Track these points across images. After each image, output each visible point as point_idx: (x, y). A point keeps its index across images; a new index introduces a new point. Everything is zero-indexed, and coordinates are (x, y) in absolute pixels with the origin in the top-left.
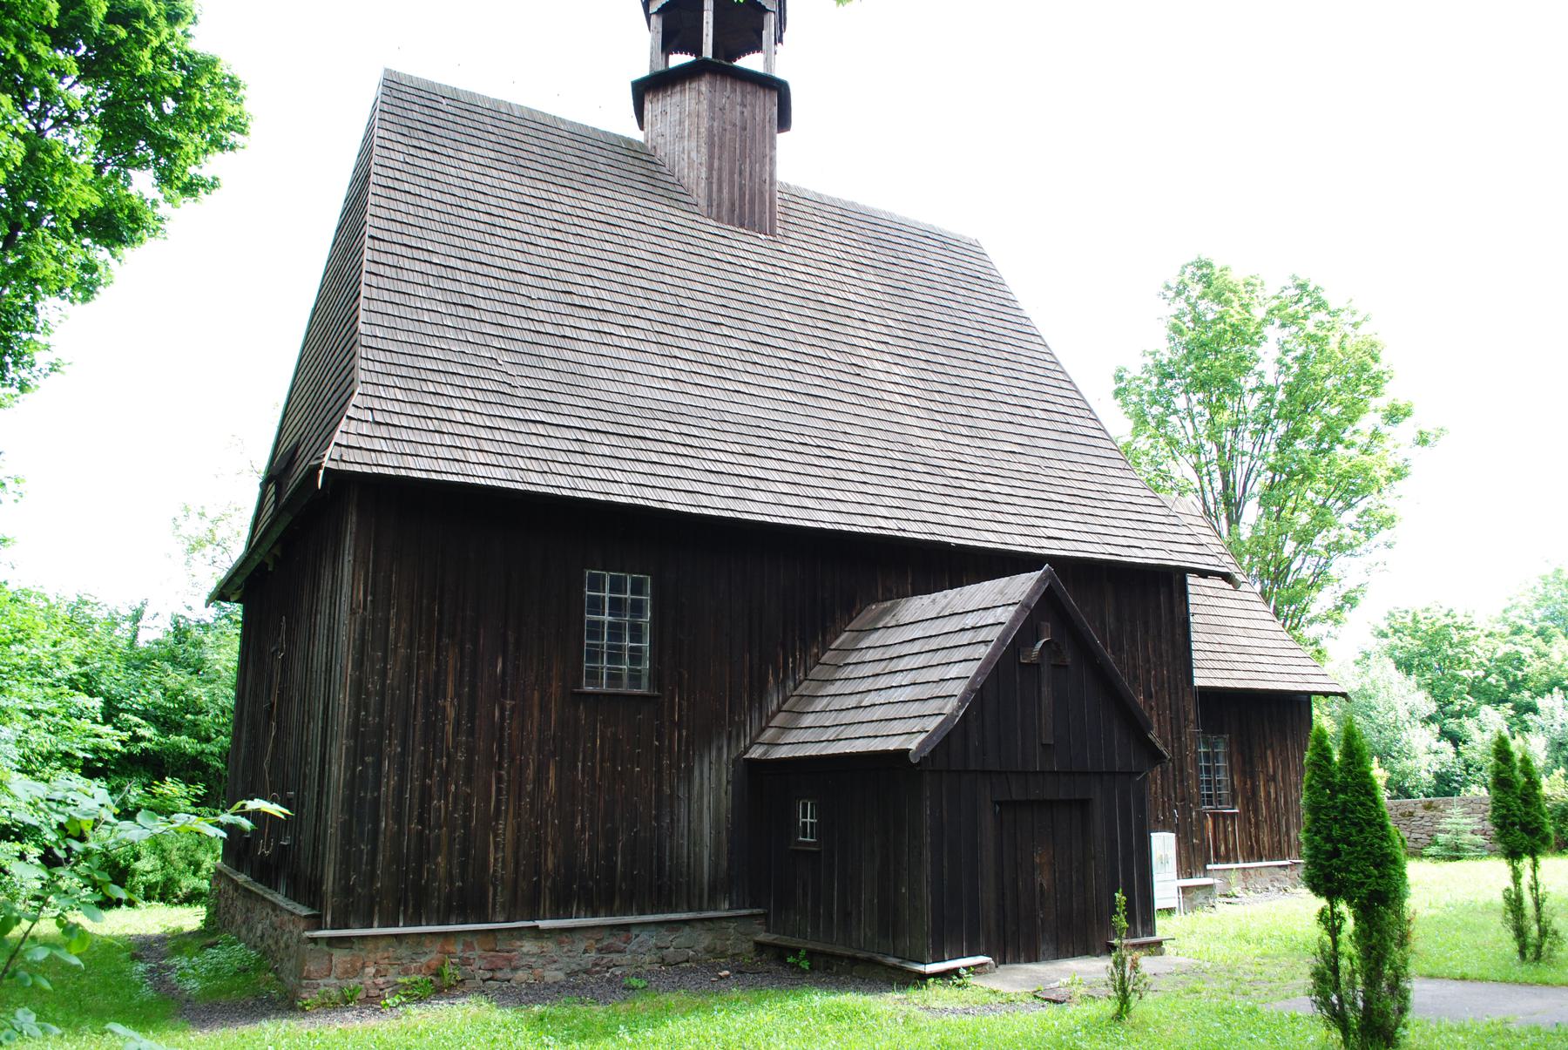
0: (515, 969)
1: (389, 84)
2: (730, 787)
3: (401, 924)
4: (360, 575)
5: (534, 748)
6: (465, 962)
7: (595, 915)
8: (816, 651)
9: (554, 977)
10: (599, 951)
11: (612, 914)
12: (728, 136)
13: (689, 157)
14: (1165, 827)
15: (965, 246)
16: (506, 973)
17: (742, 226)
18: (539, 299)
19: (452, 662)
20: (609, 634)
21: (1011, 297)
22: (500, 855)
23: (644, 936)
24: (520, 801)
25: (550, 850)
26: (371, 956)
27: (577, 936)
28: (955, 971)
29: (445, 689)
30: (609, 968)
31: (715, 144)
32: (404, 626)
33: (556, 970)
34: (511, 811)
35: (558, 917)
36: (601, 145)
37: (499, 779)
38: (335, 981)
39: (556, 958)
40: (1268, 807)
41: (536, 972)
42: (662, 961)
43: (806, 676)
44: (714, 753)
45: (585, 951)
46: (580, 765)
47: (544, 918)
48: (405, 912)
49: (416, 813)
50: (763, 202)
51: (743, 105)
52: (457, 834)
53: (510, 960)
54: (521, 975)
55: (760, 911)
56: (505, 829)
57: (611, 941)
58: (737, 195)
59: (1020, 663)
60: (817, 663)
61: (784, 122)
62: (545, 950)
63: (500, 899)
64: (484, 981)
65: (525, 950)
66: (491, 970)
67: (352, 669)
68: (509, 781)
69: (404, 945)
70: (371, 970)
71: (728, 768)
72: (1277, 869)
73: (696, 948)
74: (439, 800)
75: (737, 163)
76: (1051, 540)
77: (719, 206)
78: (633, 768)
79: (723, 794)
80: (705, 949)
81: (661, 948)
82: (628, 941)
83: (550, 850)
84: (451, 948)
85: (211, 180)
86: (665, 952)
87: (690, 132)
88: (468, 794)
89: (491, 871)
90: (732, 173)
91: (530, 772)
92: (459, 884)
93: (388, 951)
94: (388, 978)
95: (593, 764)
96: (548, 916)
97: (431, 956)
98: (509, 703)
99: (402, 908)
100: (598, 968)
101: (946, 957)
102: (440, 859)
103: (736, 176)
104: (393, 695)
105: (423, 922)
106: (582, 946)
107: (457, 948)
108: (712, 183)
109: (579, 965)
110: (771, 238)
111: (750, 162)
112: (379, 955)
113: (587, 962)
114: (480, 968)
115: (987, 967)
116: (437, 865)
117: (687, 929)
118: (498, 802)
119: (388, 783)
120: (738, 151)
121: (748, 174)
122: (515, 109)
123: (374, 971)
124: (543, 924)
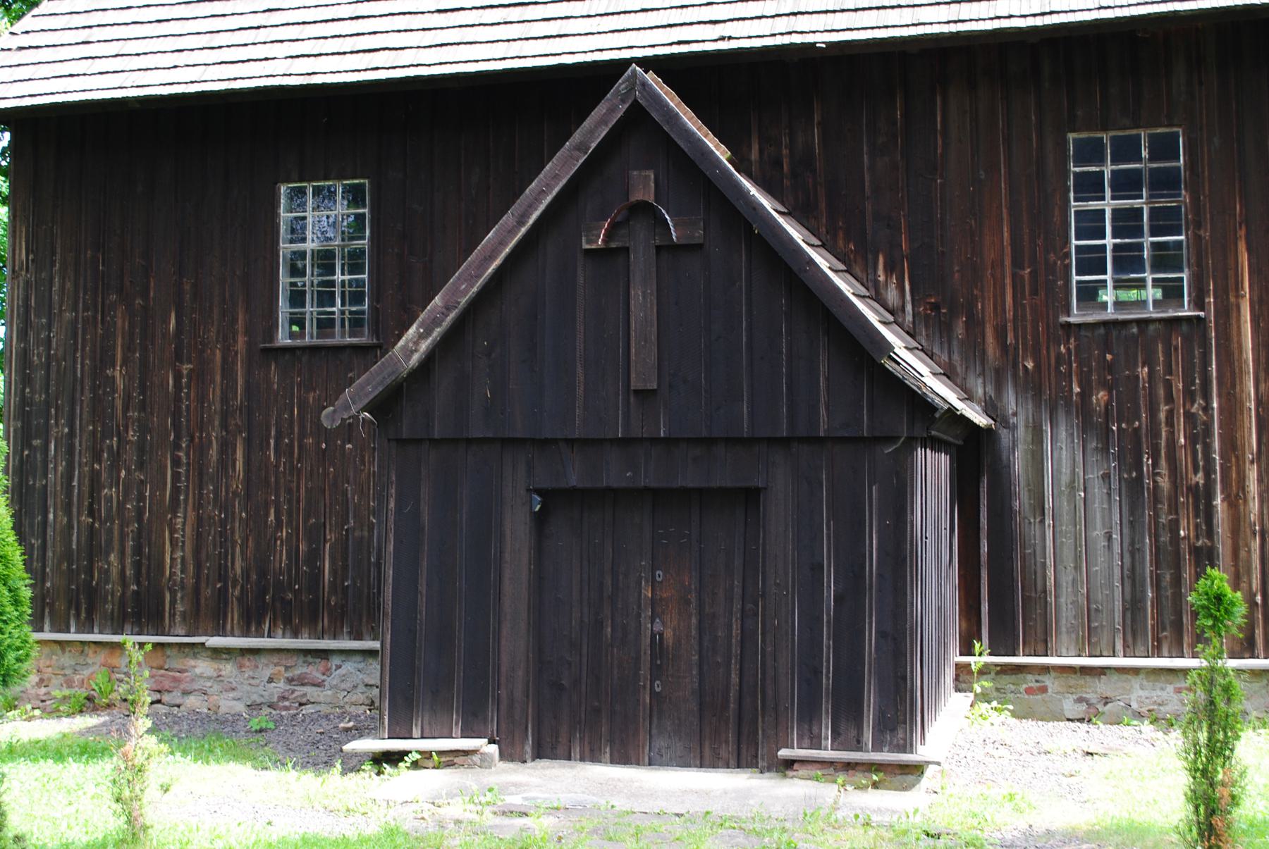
0: (186, 693)
3: (73, 629)
4: (21, 232)
5: (217, 423)
7: (296, 634)
10: (290, 681)
19: (121, 322)
22: (179, 554)
23: (349, 666)
24: (201, 488)
25: (238, 550)
27: (263, 660)
29: (114, 355)
32: (68, 285)
33: (234, 699)
34: (191, 501)
35: (246, 633)
37: (176, 462)
39: (234, 684)
45: (271, 680)
46: (272, 442)
48: (78, 615)
49: (86, 503)
52: (130, 529)
54: (192, 701)
56: (184, 524)
57: (305, 670)
62: (223, 673)
63: (180, 607)
65: (198, 671)
66: (159, 691)
68: (188, 464)
69: (67, 654)
78: (343, 446)
83: (238, 550)
88: (142, 481)
89: (168, 573)
91: (213, 453)
93: (51, 659)
95: (292, 441)
96: (236, 632)
98: (186, 368)
100: (287, 703)
104: (59, 365)
109: (262, 696)
113: (272, 694)
115: (476, 758)
116: (109, 563)
118: (176, 490)
119: (55, 468)
123: (37, 679)
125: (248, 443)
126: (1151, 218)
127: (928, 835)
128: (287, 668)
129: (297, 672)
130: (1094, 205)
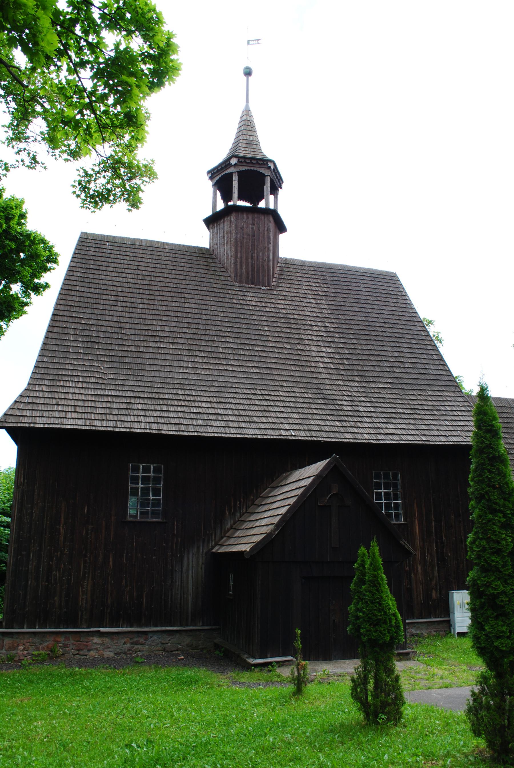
0: (89, 650)
1: (83, 240)
2: (203, 566)
6: (65, 646)
8: (252, 497)
9: (108, 655)
10: (132, 643)
11: (141, 626)
12: (245, 241)
13: (227, 254)
14: (461, 587)
15: (387, 278)
16: (85, 652)
17: (253, 284)
18: (131, 334)
20: (141, 493)
21: (409, 302)
23: (155, 637)
25: (109, 595)
26: (22, 641)
28: (270, 663)
30: (136, 652)
31: (238, 245)
33: (110, 651)
36: (185, 253)
38: (5, 652)
39: (110, 646)
41: (100, 652)
42: (164, 650)
43: (246, 510)
44: (195, 550)
45: (124, 643)
46: (125, 555)
47: (106, 627)
50: (264, 271)
51: (253, 224)
53: (87, 646)
55: (217, 627)
56: (87, 585)
58: (250, 269)
60: (253, 504)
61: (281, 228)
64: (74, 655)
65: (94, 641)
66: (78, 650)
67: (17, 512)
70: (21, 648)
71: (202, 557)
73: (182, 644)
74: (56, 572)
75: (250, 253)
77: (241, 276)
79: (200, 570)
80: (187, 645)
81: (163, 644)
82: (146, 639)
83: (109, 595)
84: (58, 639)
85: (45, 284)
86: (165, 645)
87: (227, 241)
90: (247, 259)
92: (65, 610)
94: (29, 651)
97: (49, 642)
98: (90, 527)
99: (38, 620)
100: (131, 652)
101: (268, 656)
102: (56, 598)
103: (250, 260)
105: (48, 627)
106: (123, 641)
107: (62, 639)
108: (237, 265)
110: (268, 288)
111: (257, 252)
112: (25, 641)
113: (125, 649)
114: (72, 649)
117: (178, 635)
120: (250, 247)
121: (256, 258)
122: (143, 241)
124: (102, 630)
128: (131, 639)
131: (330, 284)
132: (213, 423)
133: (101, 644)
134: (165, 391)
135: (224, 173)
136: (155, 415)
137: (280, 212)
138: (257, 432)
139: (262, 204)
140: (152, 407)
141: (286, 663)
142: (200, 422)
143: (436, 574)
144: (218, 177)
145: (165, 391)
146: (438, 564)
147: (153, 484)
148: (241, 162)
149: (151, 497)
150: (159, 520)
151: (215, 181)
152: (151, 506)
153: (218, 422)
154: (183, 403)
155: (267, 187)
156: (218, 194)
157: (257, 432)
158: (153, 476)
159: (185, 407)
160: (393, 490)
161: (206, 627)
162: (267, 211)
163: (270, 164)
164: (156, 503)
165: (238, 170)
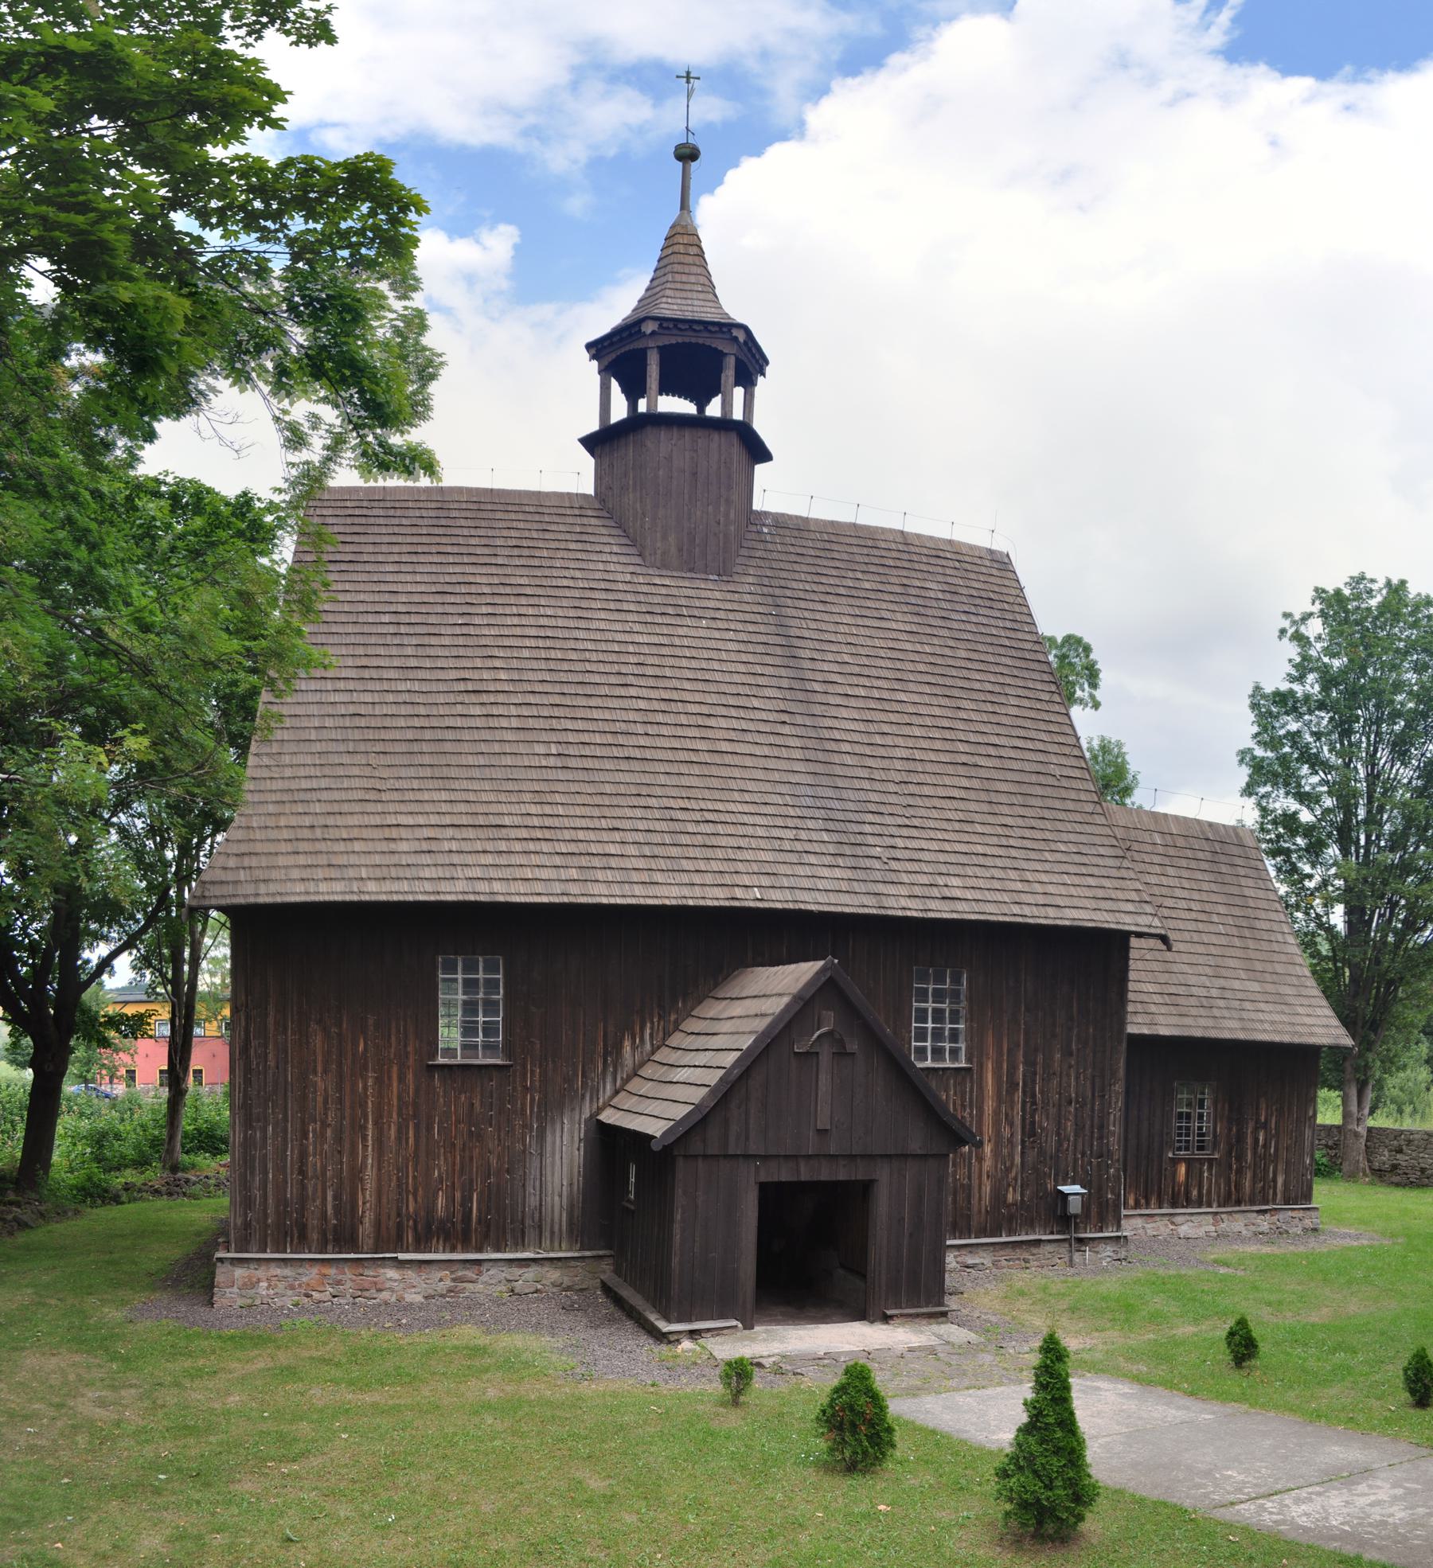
0: (380, 1290)
7: (453, 1250)
10: (454, 1280)
25: (411, 1197)
27: (434, 1267)
40: (1255, 1153)
45: (441, 1280)
47: (408, 1251)
53: (375, 1283)
59: (796, 1053)
61: (758, 452)
65: (388, 1276)
70: (264, 1284)
72: (1255, 1215)
73: (544, 1282)
76: (947, 901)
81: (509, 1281)
82: (480, 1274)
107: (332, 1271)
124: (402, 1256)
125: (417, 1127)
126: (950, 1014)
127: (1164, 939)
128: (452, 1273)
129: (460, 1274)
130: (923, 1005)
131: (863, 572)
132: (600, 875)
133: (400, 1281)
134: (504, 809)
135: (627, 348)
136: (483, 862)
137: (759, 426)
138: (686, 891)
139: (714, 409)
140: (479, 846)
141: (725, 1332)
142: (574, 873)
143: (1018, 1160)
144: (613, 356)
145: (504, 809)
146: (1023, 1142)
147: (485, 994)
148: (668, 328)
149: (481, 1019)
150: (499, 1062)
151: (606, 363)
152: (481, 1034)
153: (608, 871)
154: (539, 834)
155: (729, 374)
156: (615, 386)
157: (686, 891)
158: (485, 979)
159: (543, 842)
160: (950, 1003)
161: (588, 1253)
162: (724, 424)
163: (735, 332)
164: (489, 1029)
165: (661, 344)
